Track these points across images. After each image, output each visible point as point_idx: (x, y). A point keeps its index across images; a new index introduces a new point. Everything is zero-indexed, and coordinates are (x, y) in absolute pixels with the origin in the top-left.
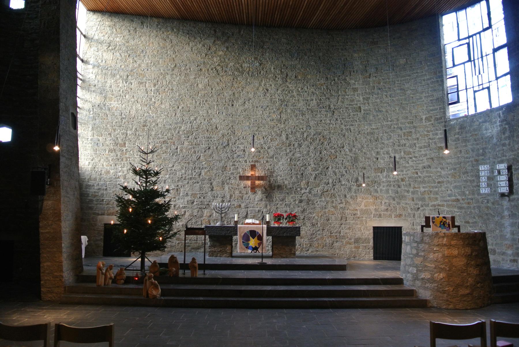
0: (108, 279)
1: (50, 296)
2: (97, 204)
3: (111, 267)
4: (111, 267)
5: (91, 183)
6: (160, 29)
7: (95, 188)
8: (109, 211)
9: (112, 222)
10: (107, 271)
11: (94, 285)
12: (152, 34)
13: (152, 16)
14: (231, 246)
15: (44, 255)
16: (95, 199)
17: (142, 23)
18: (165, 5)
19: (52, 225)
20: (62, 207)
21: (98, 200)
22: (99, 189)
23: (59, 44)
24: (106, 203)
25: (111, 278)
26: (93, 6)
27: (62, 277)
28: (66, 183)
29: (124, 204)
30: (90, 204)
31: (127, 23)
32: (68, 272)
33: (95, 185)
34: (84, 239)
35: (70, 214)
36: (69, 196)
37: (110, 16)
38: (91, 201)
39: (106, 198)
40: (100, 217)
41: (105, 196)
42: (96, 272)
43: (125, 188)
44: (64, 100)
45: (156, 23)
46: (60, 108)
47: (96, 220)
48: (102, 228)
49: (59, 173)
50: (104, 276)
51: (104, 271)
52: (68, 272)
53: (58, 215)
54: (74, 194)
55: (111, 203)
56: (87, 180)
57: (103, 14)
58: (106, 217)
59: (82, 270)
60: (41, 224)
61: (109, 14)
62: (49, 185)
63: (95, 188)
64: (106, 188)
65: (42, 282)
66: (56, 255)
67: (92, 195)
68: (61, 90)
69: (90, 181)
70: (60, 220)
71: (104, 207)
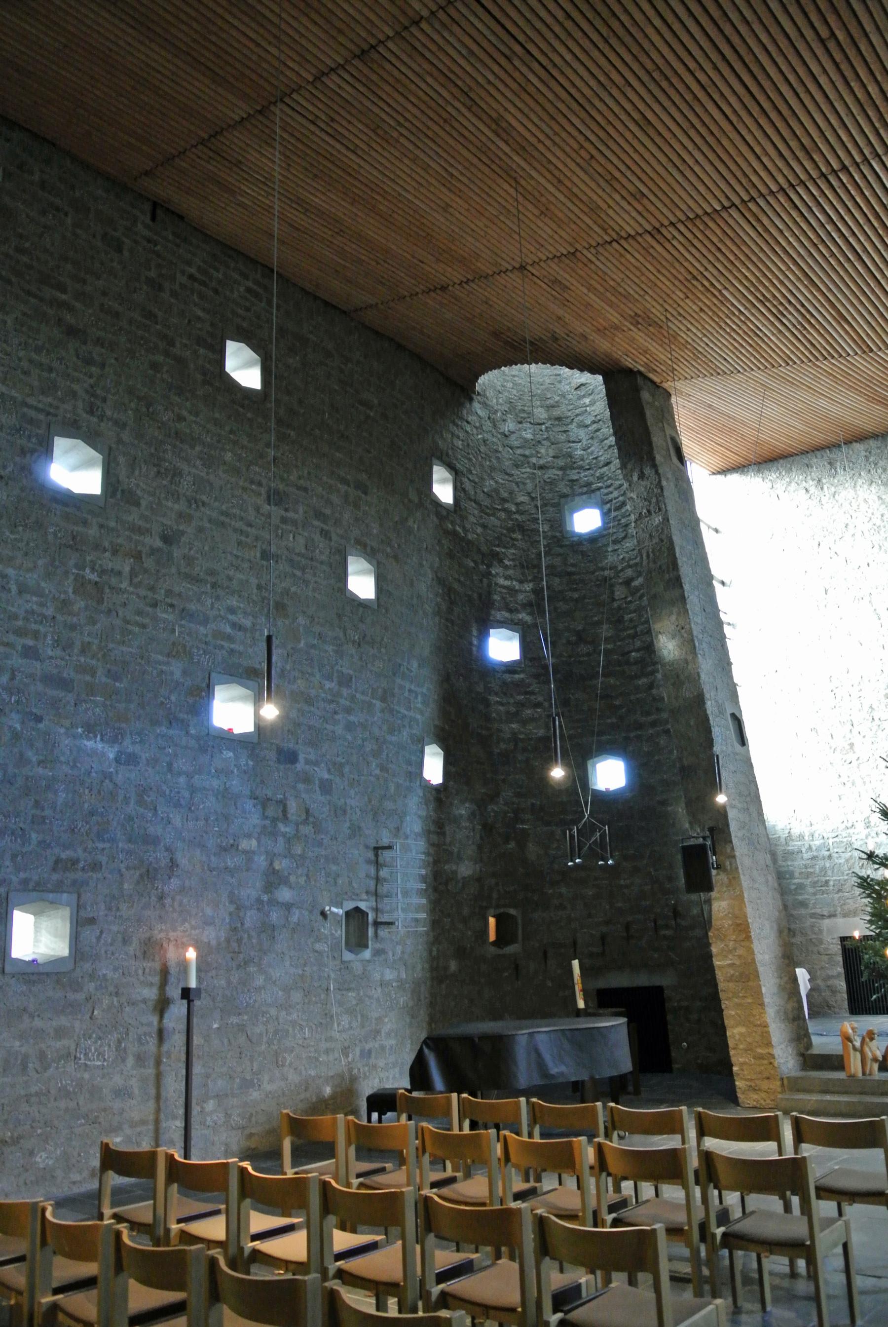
0: (869, 1062)
1: (756, 1097)
2: (815, 894)
3: (871, 1035)
4: (871, 1035)
5: (794, 846)
6: (876, 464)
7: (805, 856)
8: (846, 907)
9: (857, 934)
10: (863, 1042)
11: (841, 1075)
12: (860, 482)
13: (848, 442)
14: (815, 1305)
15: (730, 1013)
16: (808, 882)
17: (830, 463)
18: (862, 303)
19: (735, 949)
20: (749, 910)
21: (816, 883)
22: (814, 858)
23: (681, 587)
24: (836, 889)
25: (875, 1059)
26: (718, 462)
27: (773, 1056)
28: (747, 861)
29: (875, 891)
30: (801, 894)
31: (797, 476)
32: (783, 1046)
33: (804, 850)
34: (802, 974)
35: (767, 924)
36: (756, 886)
37: (759, 471)
38: (801, 886)
39: (832, 879)
40: (826, 922)
41: (829, 873)
42: (841, 1047)
43: (871, 856)
44: (713, 693)
45: (863, 453)
46: (709, 712)
47: (821, 931)
48: (836, 948)
49: (731, 842)
50: (858, 1055)
51: (858, 1044)
52: (783, 1046)
53: (743, 929)
54: (767, 881)
55: (847, 887)
56: (782, 840)
57: (743, 472)
58: (840, 921)
59: (809, 1045)
60: (714, 950)
61: (756, 468)
62: (717, 868)
63: (805, 856)
64: (827, 853)
65: (735, 1069)
66: (754, 1012)
67: (801, 873)
68: (703, 676)
69: (791, 843)
70: (748, 938)
71: (833, 899)
